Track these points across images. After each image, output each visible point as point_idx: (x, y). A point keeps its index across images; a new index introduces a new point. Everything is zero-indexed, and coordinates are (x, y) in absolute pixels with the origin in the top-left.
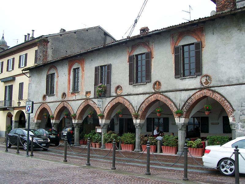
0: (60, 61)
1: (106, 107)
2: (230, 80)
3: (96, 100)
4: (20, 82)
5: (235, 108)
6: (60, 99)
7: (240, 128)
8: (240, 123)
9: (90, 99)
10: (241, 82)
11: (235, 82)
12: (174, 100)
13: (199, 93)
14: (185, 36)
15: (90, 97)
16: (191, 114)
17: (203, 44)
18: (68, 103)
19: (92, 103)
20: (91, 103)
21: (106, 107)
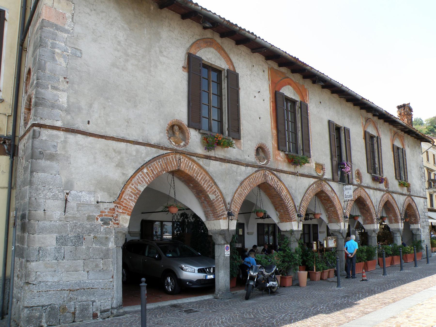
3: (334, 185)
20: (327, 188)
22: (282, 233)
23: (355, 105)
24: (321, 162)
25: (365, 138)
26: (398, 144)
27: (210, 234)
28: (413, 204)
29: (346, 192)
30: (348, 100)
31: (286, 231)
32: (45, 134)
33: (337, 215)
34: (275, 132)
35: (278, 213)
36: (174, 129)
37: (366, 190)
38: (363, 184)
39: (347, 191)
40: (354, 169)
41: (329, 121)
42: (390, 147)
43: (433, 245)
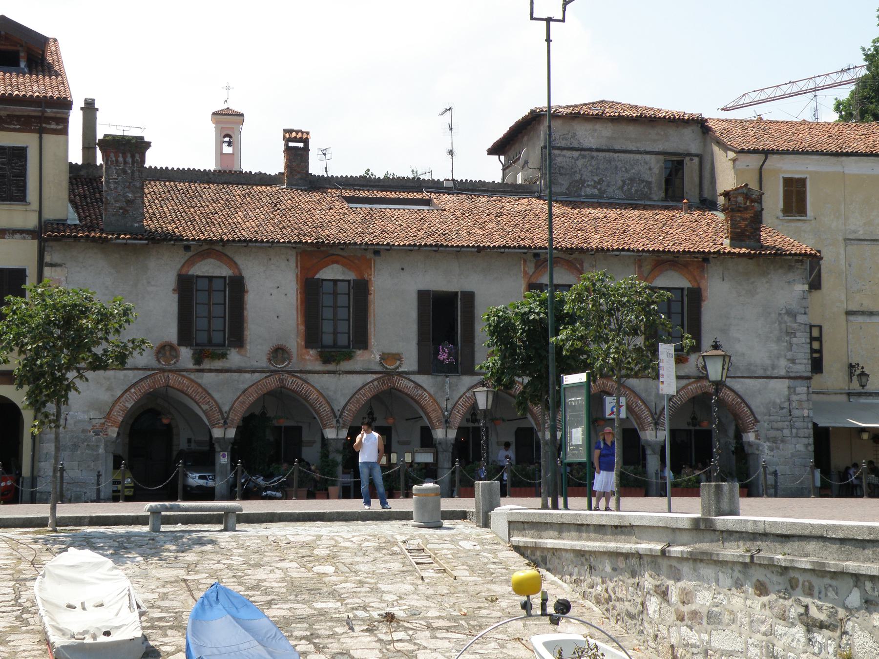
1: (460, 398)
2: (752, 368)
4: (386, 351)
5: (759, 418)
6: (263, 363)
7: (766, 451)
8: (768, 443)
9: (401, 374)
10: (769, 373)
11: (760, 373)
12: (643, 395)
13: (694, 386)
14: (667, 270)
15: (400, 370)
16: (331, 234)
17: (704, 294)
18: (306, 381)
19: (411, 385)
21: (460, 398)
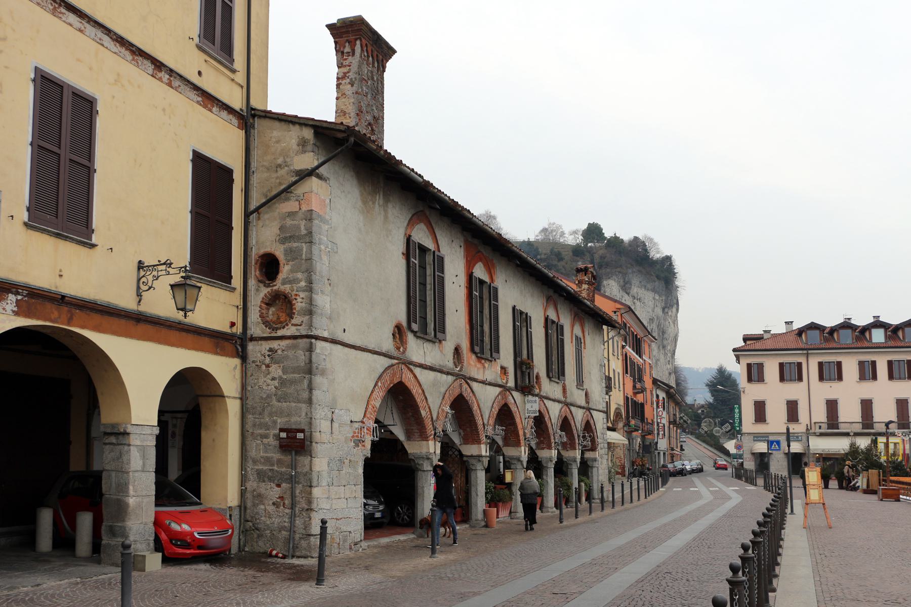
0: (193, 94)
3: (516, 394)
22: (465, 459)
23: (537, 279)
24: (505, 365)
25: (407, 255)
26: (480, 272)
27: (410, 457)
28: (592, 422)
29: (528, 406)
30: (531, 275)
31: (472, 456)
32: (320, 345)
33: (518, 435)
34: (468, 327)
35: (461, 431)
36: (399, 332)
37: (417, 371)
38: (542, 393)
39: (530, 405)
40: (536, 371)
41: (514, 308)
42: (462, 280)
43: (903, 422)
